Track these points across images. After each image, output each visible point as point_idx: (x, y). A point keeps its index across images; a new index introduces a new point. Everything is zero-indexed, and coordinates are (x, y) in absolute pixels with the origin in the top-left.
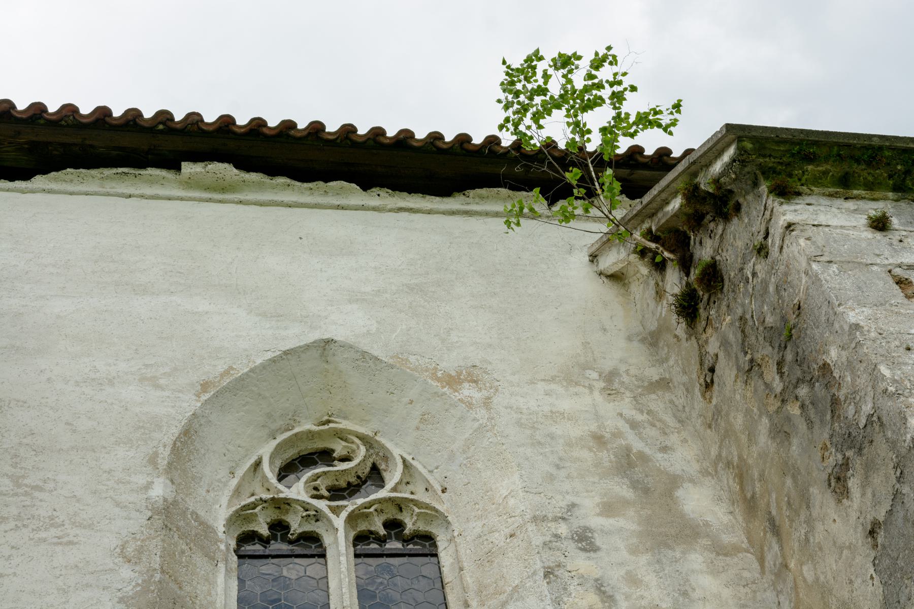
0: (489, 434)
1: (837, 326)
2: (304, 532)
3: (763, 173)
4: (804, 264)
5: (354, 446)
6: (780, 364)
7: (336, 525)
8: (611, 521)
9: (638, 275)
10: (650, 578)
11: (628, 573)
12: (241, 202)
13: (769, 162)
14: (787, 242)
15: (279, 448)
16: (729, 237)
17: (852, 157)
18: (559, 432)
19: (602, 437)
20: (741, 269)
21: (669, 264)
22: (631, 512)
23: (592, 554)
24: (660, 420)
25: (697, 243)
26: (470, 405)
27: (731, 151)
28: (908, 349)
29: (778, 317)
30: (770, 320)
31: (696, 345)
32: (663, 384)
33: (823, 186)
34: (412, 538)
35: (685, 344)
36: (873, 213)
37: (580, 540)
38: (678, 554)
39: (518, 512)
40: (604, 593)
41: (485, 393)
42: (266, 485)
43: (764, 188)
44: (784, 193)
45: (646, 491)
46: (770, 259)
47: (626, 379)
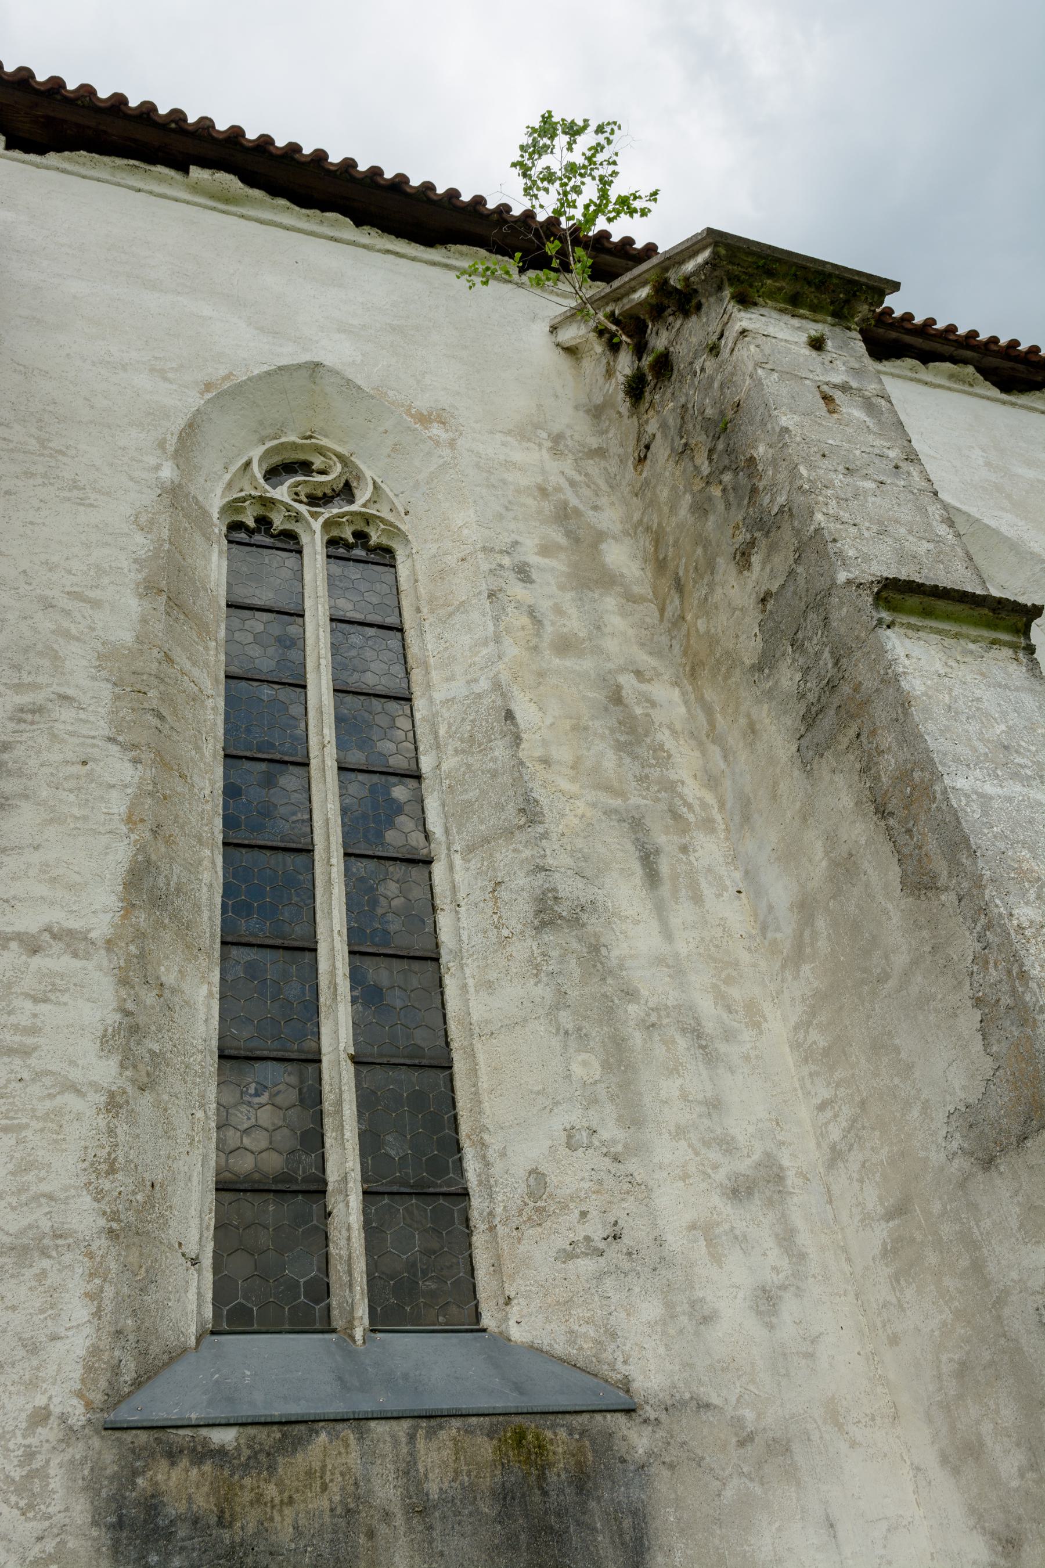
0: (451, 471)
1: (769, 426)
2: (285, 530)
3: (729, 280)
4: (751, 368)
5: (331, 463)
6: (711, 451)
7: (314, 528)
8: (547, 561)
9: (592, 352)
10: (573, 611)
11: (556, 604)
13: (736, 270)
14: (738, 345)
15: (267, 454)
16: (685, 332)
17: (806, 279)
18: (510, 479)
19: (546, 489)
20: (691, 363)
21: (624, 346)
22: (563, 556)
23: (528, 585)
24: (594, 483)
25: (654, 333)
26: (437, 443)
27: (706, 254)
28: (824, 456)
29: (718, 411)
30: (709, 412)
31: (636, 423)
32: (600, 453)
33: (776, 300)
34: (375, 549)
35: (626, 420)
36: (813, 333)
37: (519, 572)
38: (596, 596)
39: (470, 541)
40: (535, 617)
41: (451, 435)
42: (254, 484)
43: (727, 293)
44: (744, 301)
45: (577, 540)
46: (720, 358)
47: (570, 443)
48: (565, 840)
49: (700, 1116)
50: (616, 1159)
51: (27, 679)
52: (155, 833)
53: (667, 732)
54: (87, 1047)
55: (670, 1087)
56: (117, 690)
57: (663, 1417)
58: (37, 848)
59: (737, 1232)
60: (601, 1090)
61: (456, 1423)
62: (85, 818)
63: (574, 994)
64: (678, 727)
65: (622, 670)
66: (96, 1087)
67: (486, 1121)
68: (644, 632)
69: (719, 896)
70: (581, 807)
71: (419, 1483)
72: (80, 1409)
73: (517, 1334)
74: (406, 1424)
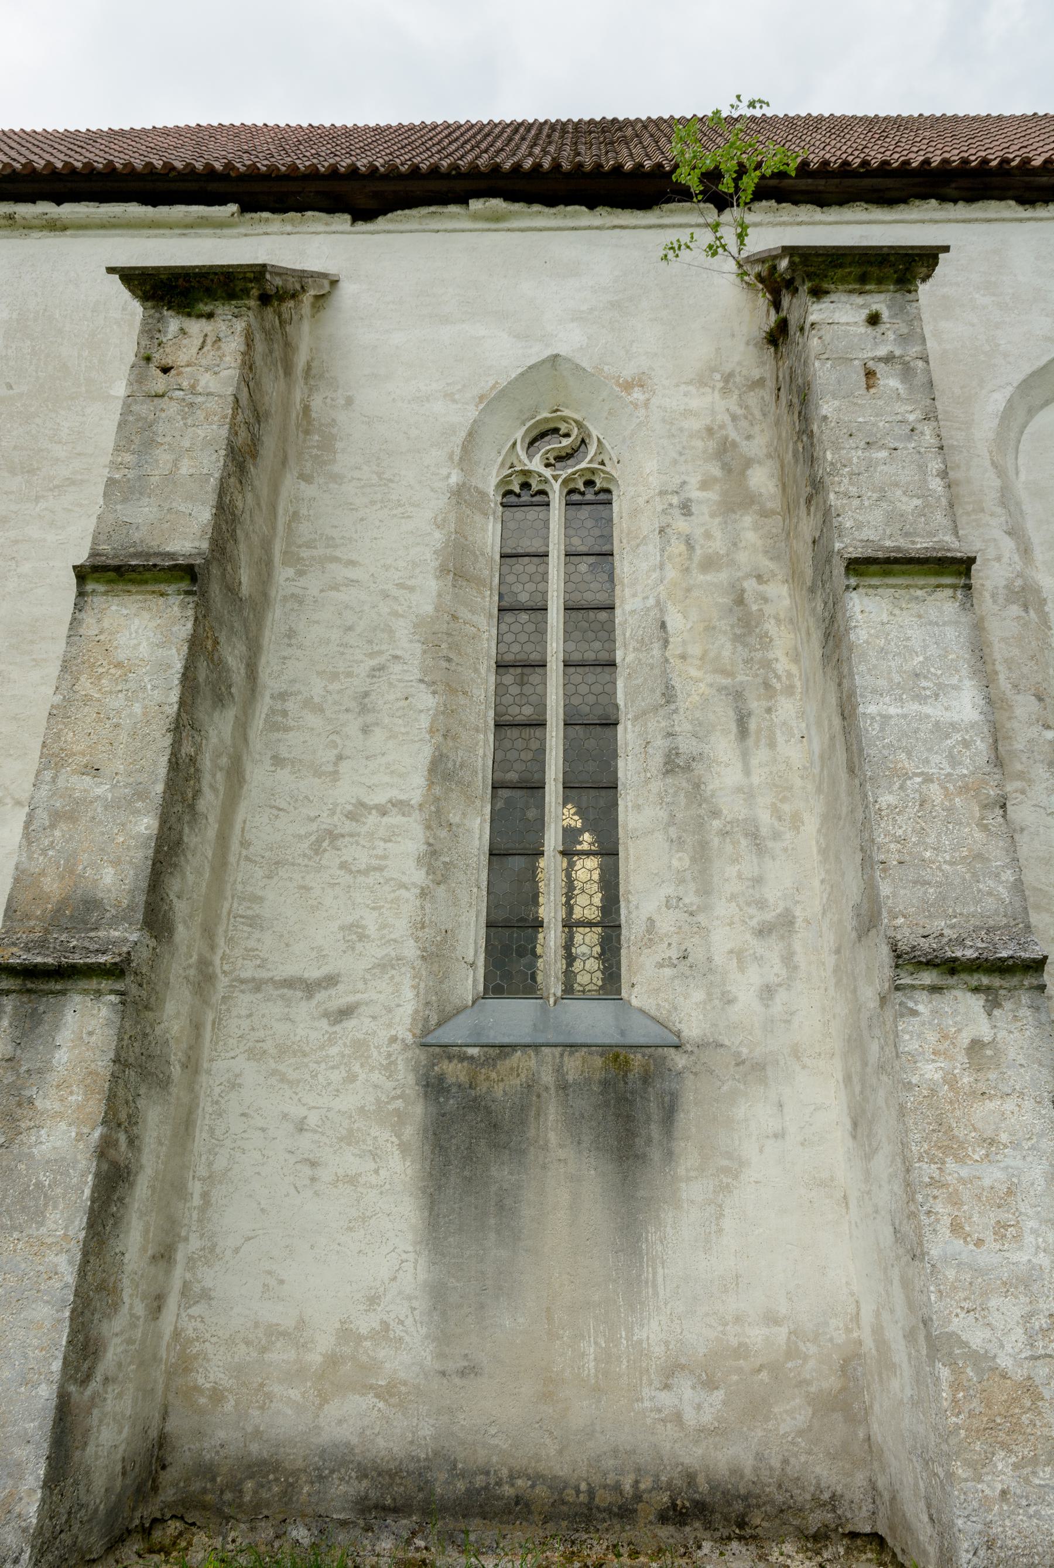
8: (704, 494)
10: (718, 534)
12: (509, 230)
18: (686, 426)
23: (688, 518)
24: (751, 414)
26: (636, 406)
37: (683, 508)
38: (738, 517)
41: (647, 395)
44: (818, 293)
45: (730, 471)
48: (688, 713)
49: (747, 887)
50: (692, 914)
51: (376, 648)
52: (445, 736)
53: (773, 621)
54: (411, 864)
55: (732, 871)
56: (424, 647)
57: (696, 1050)
58: (383, 755)
59: (757, 955)
60: (688, 875)
61: (585, 1049)
62: (407, 733)
63: (679, 816)
64: (782, 616)
65: (747, 576)
66: (414, 885)
67: (630, 888)
68: (769, 541)
69: (787, 741)
70: (702, 687)
71: (563, 1075)
72: (410, 1037)
73: (635, 1002)
74: (559, 1049)
